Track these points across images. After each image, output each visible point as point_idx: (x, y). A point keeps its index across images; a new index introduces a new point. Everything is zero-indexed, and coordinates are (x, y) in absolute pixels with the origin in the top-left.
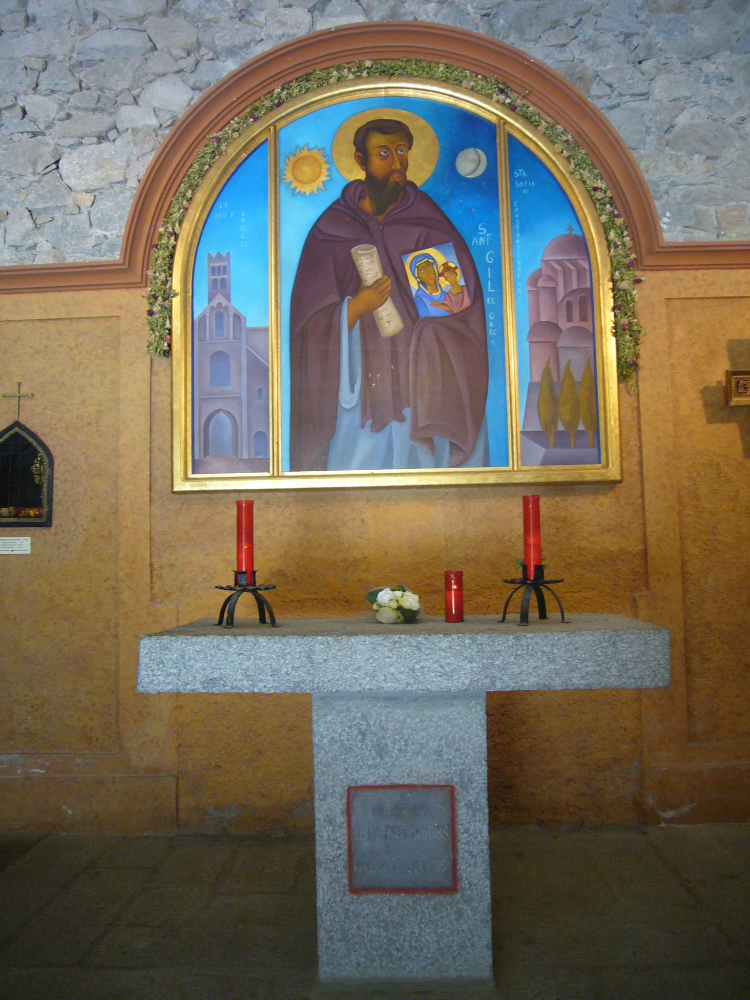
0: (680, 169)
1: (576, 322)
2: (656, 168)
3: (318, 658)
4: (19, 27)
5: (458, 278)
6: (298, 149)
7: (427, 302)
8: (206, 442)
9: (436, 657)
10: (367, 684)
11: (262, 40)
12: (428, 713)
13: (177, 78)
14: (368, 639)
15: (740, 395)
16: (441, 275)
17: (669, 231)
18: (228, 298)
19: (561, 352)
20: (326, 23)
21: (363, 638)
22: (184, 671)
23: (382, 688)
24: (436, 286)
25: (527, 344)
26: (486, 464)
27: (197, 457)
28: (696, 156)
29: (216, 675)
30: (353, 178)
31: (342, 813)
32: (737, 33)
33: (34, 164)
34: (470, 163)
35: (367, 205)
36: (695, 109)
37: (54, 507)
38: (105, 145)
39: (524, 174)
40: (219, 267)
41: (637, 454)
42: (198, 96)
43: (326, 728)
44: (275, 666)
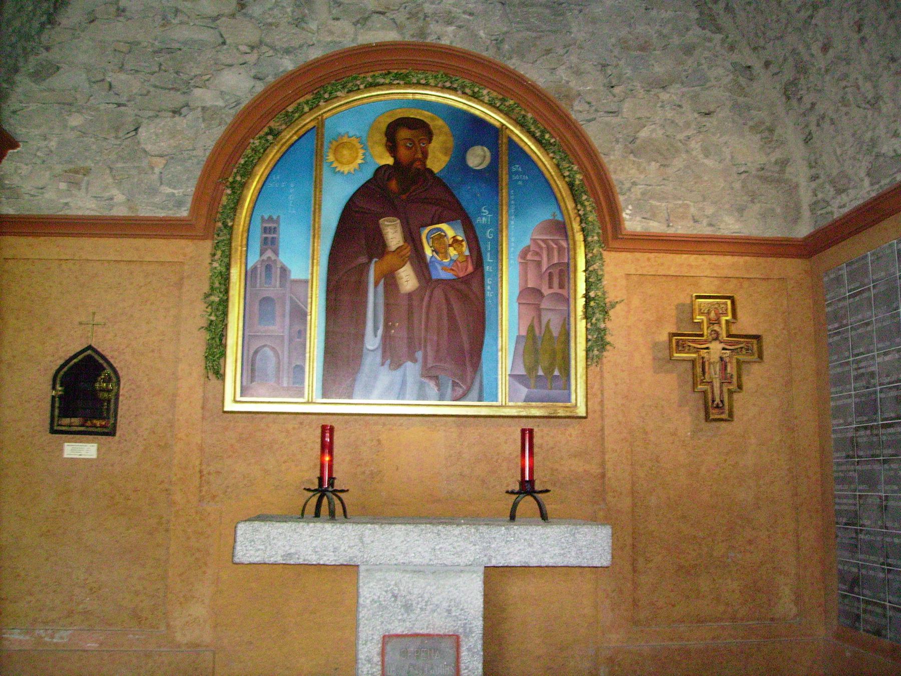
0: (641, 173)
1: (556, 289)
2: (622, 170)
3: (367, 540)
4: (111, 16)
6: (340, 136)
7: (439, 267)
9: (450, 541)
10: (401, 559)
11: (313, 45)
12: (442, 582)
14: (403, 527)
15: (680, 352)
16: (450, 246)
17: (630, 220)
18: (276, 253)
19: (543, 313)
21: (400, 526)
22: (269, 547)
24: (446, 255)
25: (516, 305)
26: (480, 400)
27: (245, 384)
28: (653, 163)
29: (293, 551)
31: (378, 654)
32: (685, 71)
33: (117, 129)
34: (478, 157)
35: (393, 185)
36: (653, 126)
37: (119, 419)
38: (177, 118)
39: (520, 169)
40: (270, 228)
41: (600, 396)
42: (260, 87)
43: (370, 590)
44: (336, 545)
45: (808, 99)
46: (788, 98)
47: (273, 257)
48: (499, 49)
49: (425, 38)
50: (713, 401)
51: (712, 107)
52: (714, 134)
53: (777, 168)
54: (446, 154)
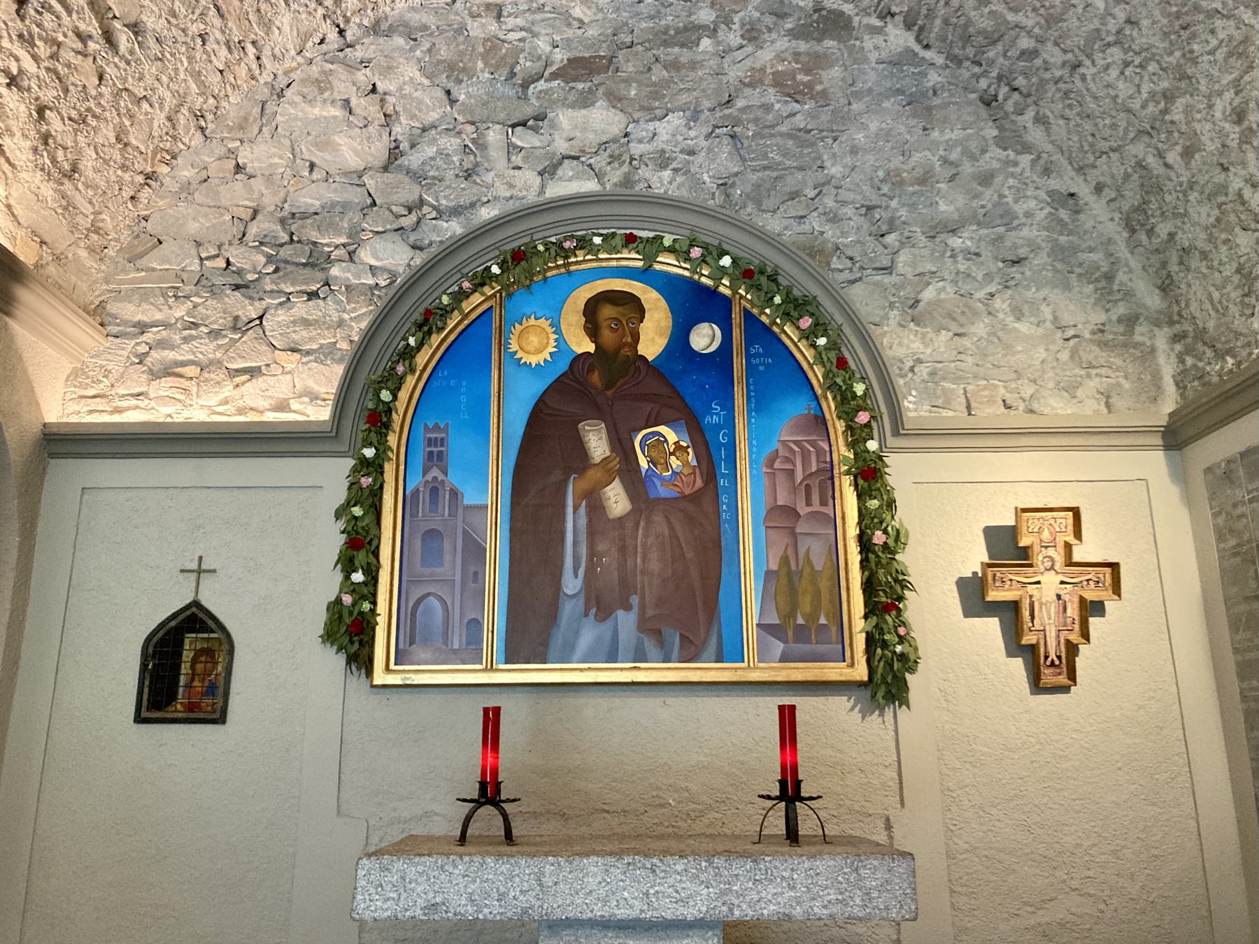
0: (926, 346)
1: (816, 506)
2: (900, 344)
5: (690, 458)
7: (658, 483)
8: (413, 628)
9: (671, 881)
10: (599, 911)
13: (396, 237)
16: (671, 454)
19: (799, 538)
20: (556, 190)
22: (404, 895)
23: (615, 915)
24: (667, 466)
27: (401, 646)
28: (944, 332)
29: (438, 900)
30: (580, 350)
32: (983, 207)
34: (704, 338)
35: (595, 378)
36: (941, 284)
44: (502, 889)
45: (1163, 229)
46: (1133, 231)
47: (441, 477)
48: (727, 196)
49: (632, 187)
50: (1046, 657)
51: (1022, 252)
52: (1028, 288)
53: (1121, 329)
54: (661, 335)
